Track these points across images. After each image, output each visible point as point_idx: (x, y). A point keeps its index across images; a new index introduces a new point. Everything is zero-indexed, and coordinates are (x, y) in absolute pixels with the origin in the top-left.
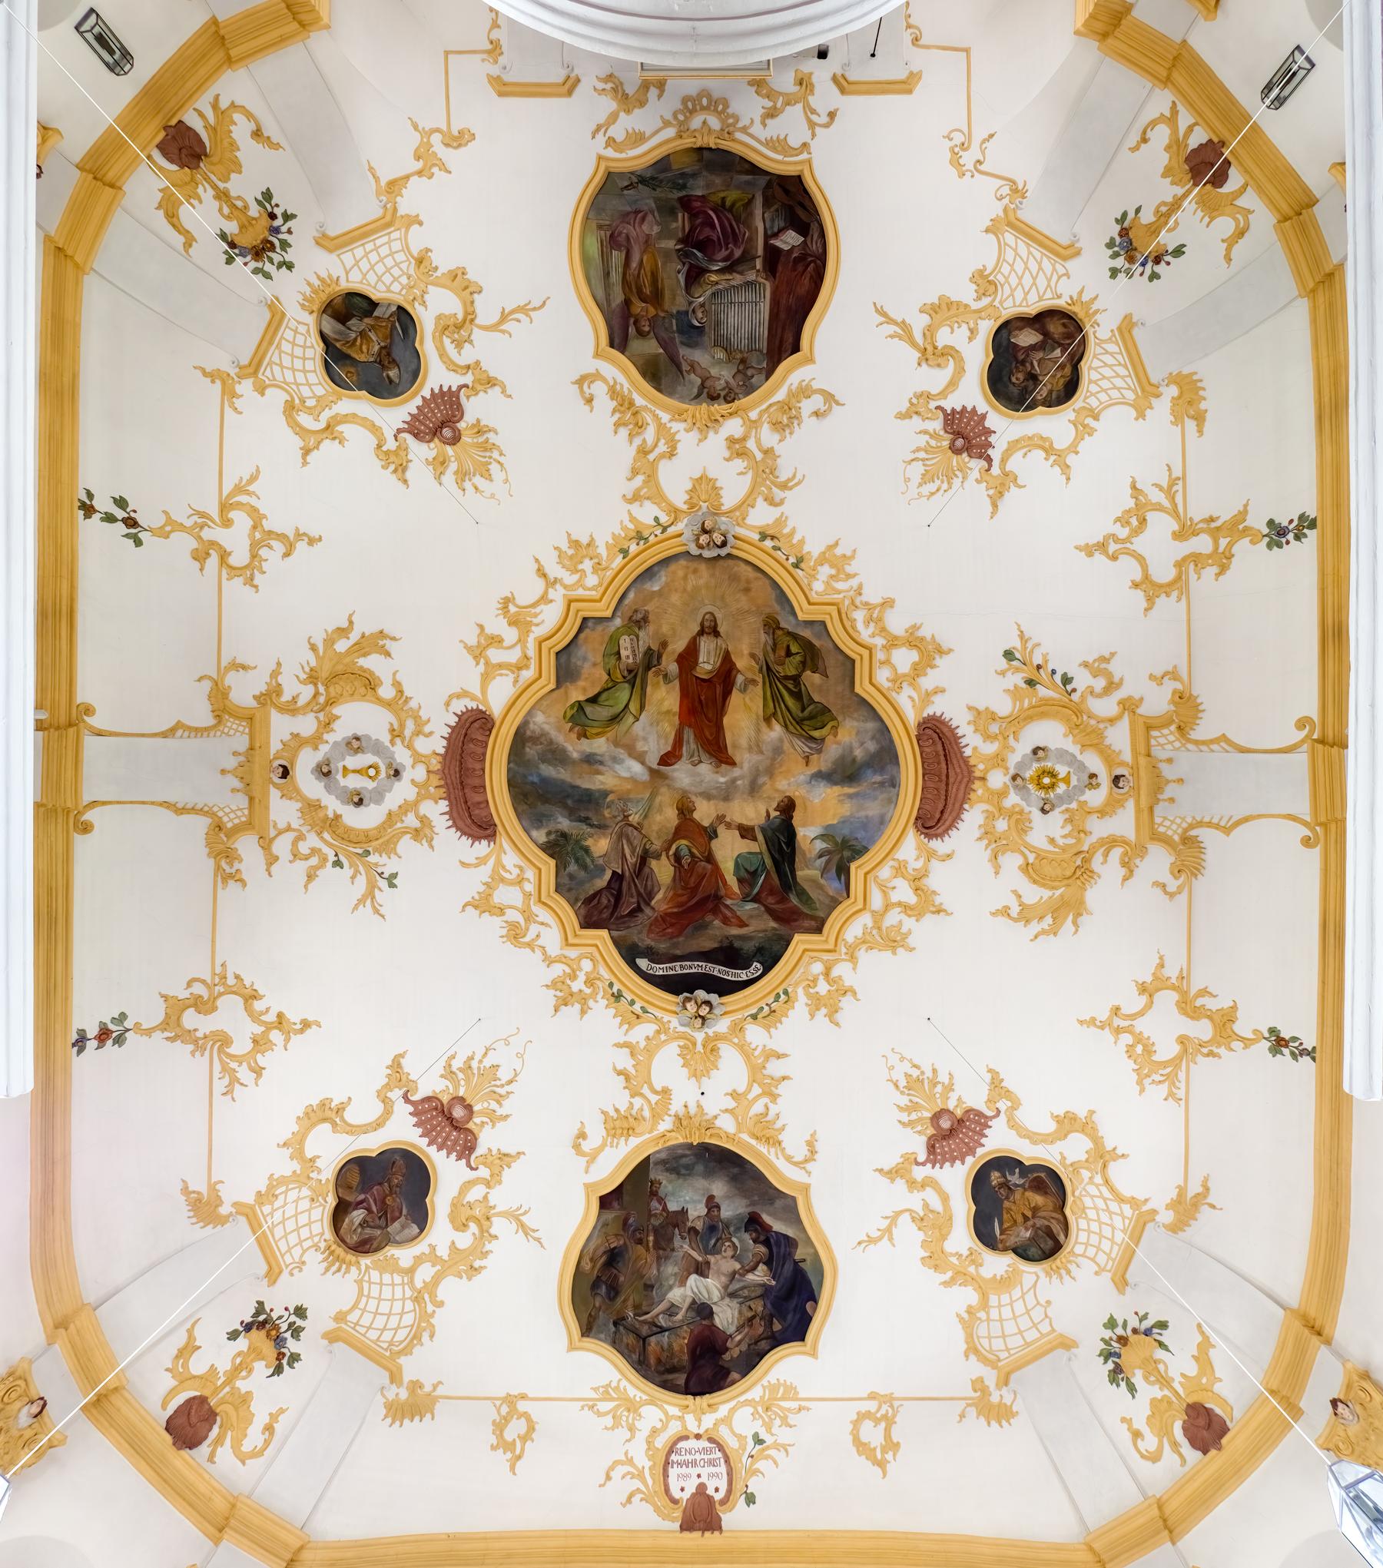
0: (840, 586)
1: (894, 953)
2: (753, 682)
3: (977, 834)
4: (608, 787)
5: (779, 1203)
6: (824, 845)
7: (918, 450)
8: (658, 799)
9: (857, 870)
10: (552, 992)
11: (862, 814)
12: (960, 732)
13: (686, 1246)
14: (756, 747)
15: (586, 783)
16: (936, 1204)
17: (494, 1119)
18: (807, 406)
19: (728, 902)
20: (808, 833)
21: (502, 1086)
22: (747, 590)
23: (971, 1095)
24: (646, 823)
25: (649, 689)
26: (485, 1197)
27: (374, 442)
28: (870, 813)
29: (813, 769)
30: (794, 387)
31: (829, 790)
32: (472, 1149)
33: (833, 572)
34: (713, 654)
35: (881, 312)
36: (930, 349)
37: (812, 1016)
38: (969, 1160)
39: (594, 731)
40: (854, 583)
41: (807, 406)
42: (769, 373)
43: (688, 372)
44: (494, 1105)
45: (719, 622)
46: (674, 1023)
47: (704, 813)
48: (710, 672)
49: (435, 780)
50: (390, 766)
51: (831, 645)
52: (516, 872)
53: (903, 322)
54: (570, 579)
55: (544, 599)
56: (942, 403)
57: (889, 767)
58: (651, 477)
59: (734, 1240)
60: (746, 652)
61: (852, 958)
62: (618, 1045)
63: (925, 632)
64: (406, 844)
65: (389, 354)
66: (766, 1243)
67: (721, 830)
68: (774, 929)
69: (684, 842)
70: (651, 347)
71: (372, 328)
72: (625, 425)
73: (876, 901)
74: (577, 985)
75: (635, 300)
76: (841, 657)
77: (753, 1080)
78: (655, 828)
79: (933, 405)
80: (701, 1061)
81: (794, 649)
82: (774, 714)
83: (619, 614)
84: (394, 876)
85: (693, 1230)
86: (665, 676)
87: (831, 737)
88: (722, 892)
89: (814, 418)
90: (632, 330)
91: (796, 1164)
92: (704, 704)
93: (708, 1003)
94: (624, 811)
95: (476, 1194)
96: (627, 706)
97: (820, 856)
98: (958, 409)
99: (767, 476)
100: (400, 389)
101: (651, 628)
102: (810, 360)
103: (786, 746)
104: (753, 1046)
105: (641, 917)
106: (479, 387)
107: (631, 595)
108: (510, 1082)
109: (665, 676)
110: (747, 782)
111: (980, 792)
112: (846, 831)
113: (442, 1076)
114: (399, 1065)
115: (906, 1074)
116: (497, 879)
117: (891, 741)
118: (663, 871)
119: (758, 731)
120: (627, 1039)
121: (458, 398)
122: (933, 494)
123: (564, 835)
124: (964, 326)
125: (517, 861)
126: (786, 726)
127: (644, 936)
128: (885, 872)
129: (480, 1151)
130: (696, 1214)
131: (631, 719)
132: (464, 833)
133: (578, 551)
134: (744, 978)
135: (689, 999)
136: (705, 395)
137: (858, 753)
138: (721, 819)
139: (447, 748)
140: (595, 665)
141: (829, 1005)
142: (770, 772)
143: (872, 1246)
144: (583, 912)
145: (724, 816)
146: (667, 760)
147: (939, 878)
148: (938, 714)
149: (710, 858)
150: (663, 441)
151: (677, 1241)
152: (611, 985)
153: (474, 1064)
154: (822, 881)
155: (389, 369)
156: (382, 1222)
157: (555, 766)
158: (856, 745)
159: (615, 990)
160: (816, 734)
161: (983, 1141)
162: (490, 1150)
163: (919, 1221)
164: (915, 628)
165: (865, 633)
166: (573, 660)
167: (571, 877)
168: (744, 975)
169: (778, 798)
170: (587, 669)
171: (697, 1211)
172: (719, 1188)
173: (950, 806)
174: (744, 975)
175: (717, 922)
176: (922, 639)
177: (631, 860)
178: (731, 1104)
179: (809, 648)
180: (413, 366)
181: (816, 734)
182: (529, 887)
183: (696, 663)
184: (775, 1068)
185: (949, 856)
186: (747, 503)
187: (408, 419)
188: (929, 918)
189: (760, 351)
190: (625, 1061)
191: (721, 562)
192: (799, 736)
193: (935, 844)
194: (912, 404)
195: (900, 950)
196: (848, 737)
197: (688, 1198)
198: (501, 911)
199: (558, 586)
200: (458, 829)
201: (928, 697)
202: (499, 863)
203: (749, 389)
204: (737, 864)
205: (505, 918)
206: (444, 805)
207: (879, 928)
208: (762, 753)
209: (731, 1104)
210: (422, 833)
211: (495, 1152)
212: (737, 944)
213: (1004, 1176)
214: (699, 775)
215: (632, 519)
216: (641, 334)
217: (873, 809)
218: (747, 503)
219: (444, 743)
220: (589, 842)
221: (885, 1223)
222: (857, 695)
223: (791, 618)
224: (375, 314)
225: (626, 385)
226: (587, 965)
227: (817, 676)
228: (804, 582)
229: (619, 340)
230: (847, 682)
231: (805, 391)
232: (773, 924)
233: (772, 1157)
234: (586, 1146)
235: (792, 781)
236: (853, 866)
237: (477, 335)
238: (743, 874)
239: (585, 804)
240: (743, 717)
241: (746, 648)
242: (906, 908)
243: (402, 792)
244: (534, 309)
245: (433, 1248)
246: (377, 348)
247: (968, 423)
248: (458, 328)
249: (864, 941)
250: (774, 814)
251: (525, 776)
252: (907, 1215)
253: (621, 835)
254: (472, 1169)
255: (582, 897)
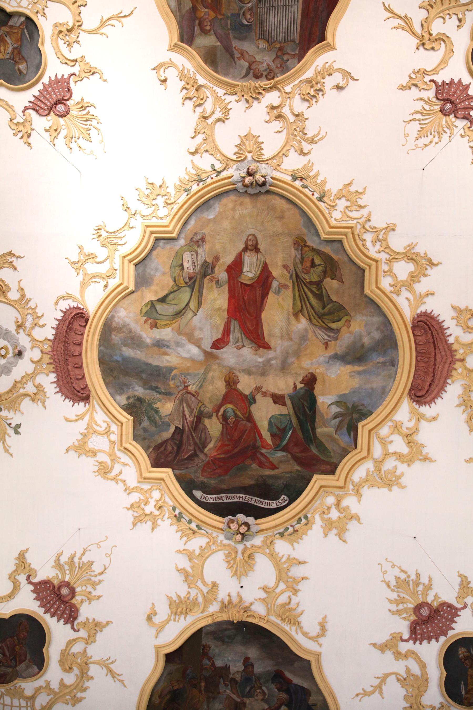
0: (354, 214)
1: (390, 490)
2: (285, 286)
3: (457, 402)
4: (172, 365)
5: (297, 665)
6: (338, 410)
7: (416, 112)
8: (211, 374)
9: (363, 428)
10: (131, 512)
11: (368, 386)
12: (445, 325)
13: (228, 691)
14: (287, 335)
15: (156, 362)
16: (416, 670)
17: (90, 599)
18: (329, 82)
19: (263, 451)
20: (325, 400)
21: (96, 576)
22: (281, 218)
23: (446, 593)
24: (201, 392)
25: (205, 292)
26: (85, 651)
27: (8, 116)
28: (375, 386)
29: (330, 352)
30: (319, 68)
31: (343, 368)
32: (75, 618)
33: (348, 204)
34: (254, 265)
35: (388, 10)
36: (426, 36)
37: (326, 535)
38: (442, 639)
39: (163, 323)
40: (364, 212)
41: (329, 82)
42: (301, 57)
43: (239, 59)
44: (90, 589)
45: (259, 241)
46: (221, 538)
47: (246, 385)
48: (252, 279)
49: (47, 359)
50: (15, 347)
51: (346, 259)
52: (104, 426)
53: (406, 16)
54: (146, 211)
55: (127, 226)
56: (435, 77)
57: (390, 351)
58: (209, 138)
59: (264, 688)
60: (280, 264)
61: (358, 494)
62: (180, 552)
63: (420, 249)
64: (26, 402)
65: (19, 53)
66: (287, 691)
67: (259, 397)
68: (298, 471)
69: (230, 406)
70: (209, 41)
71: (8, 34)
72: (190, 99)
73: (377, 451)
74: (149, 508)
75: (199, 7)
76: (354, 268)
77: (280, 579)
78: (208, 395)
79: (427, 79)
80: (242, 566)
81: (318, 261)
82: (301, 311)
83: (183, 236)
84: (18, 426)
85: (233, 680)
86: (217, 282)
87: (345, 328)
88: (259, 443)
89: (335, 91)
90: (197, 29)
91: (311, 638)
92: (246, 306)
93: (247, 524)
94: (184, 382)
95: (77, 648)
96: (188, 304)
97: (335, 418)
98: (448, 81)
99: (298, 134)
100: (27, 78)
101: (207, 246)
102: (331, 47)
103: (310, 334)
104: (280, 555)
105: (197, 461)
106: (84, 75)
107: (192, 222)
108: (101, 574)
109: (217, 282)
110: (279, 362)
111: (460, 370)
112: (355, 399)
113: (53, 567)
114: (24, 557)
115: (396, 578)
116: (90, 430)
117: (392, 332)
118: (214, 427)
119: (289, 323)
120: (187, 547)
121: (68, 83)
122: (426, 146)
123: (140, 400)
124: (454, 17)
125: (106, 419)
126: (310, 320)
127: (199, 474)
128: (384, 431)
129: (81, 619)
130: (236, 669)
131: (190, 314)
132: (67, 397)
133: (154, 190)
134: (274, 506)
135: (233, 521)
136: (251, 75)
137: (366, 340)
138: (258, 389)
139: (56, 335)
140: (164, 274)
141: (338, 528)
142: (298, 354)
143: (366, 698)
144: (153, 455)
145: (261, 387)
146: (217, 345)
147: (427, 435)
148: (429, 311)
149: (250, 418)
150: (219, 109)
151: (222, 688)
152: (174, 509)
153: (76, 560)
154: (336, 436)
155: (21, 64)
156: (13, 663)
157: (133, 348)
158: (364, 334)
159: (177, 512)
160: (334, 326)
161: (454, 625)
162: (88, 619)
163: (403, 681)
164: (411, 247)
165: (373, 251)
166: (148, 270)
167: (145, 430)
168: (274, 504)
169: (303, 374)
170: (158, 277)
171: (236, 667)
172: (253, 653)
173: (436, 381)
174: (274, 504)
175: (254, 466)
176: (417, 254)
177: (190, 418)
178: (263, 595)
179: (327, 259)
180: (37, 61)
181: (334, 326)
182: (114, 437)
183: (241, 271)
184: (296, 572)
185: (435, 419)
186: (282, 154)
187: (33, 99)
188: (417, 465)
189: (294, 41)
190: (185, 564)
191: (262, 198)
192: (321, 327)
193: (424, 409)
194: (411, 78)
195: (395, 488)
196: (359, 328)
197: (230, 659)
198: (94, 453)
199: (138, 217)
200: (63, 394)
201: (421, 298)
202: (92, 418)
203: (284, 69)
204: (270, 423)
205: (97, 459)
206: (53, 377)
207: (380, 471)
208: (291, 340)
209: (263, 595)
210: (38, 396)
211: (91, 621)
212: (269, 482)
213: (469, 652)
214: (242, 356)
215: (194, 167)
216: (204, 32)
217: (376, 383)
218: (282, 154)
219: (54, 332)
220: (158, 405)
221: (376, 682)
222: (366, 296)
223: (316, 238)
224: (10, 23)
225: (192, 69)
226: (156, 495)
227: (335, 282)
228: (326, 212)
229: (187, 36)
230: (358, 286)
231: (328, 72)
232: (297, 467)
233: (293, 633)
234: (156, 620)
235: (314, 361)
236: (360, 425)
237: (83, 37)
238: (275, 430)
239: (155, 377)
240: (277, 314)
241: (279, 258)
242: (400, 457)
243: (24, 367)
244: (125, 16)
245: (48, 683)
246: (11, 49)
247: (455, 92)
248: (68, 32)
249: (368, 481)
250: (300, 386)
251: (111, 356)
252: (393, 677)
253: (181, 401)
254: (75, 630)
255: (153, 445)
